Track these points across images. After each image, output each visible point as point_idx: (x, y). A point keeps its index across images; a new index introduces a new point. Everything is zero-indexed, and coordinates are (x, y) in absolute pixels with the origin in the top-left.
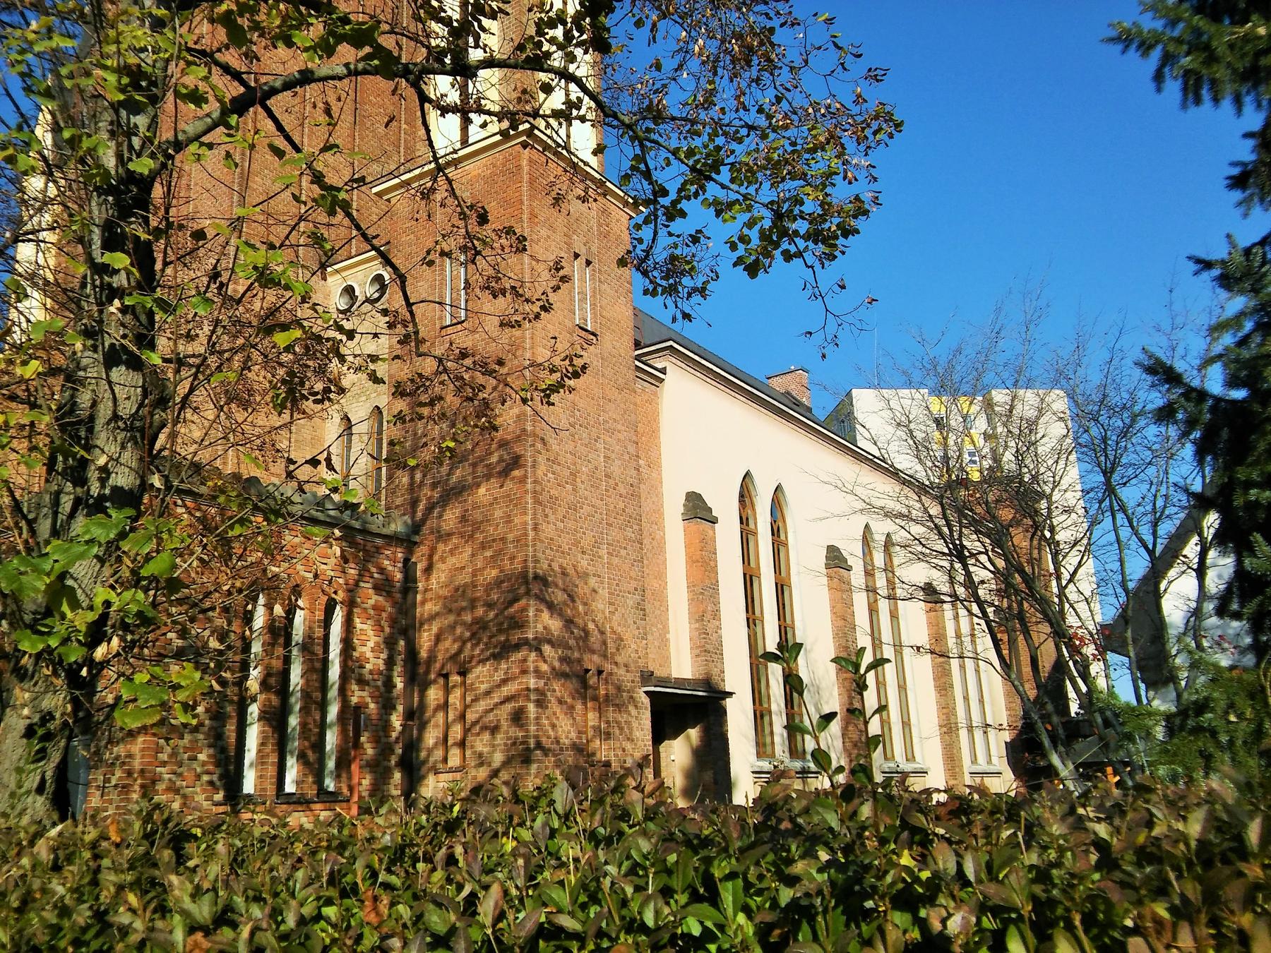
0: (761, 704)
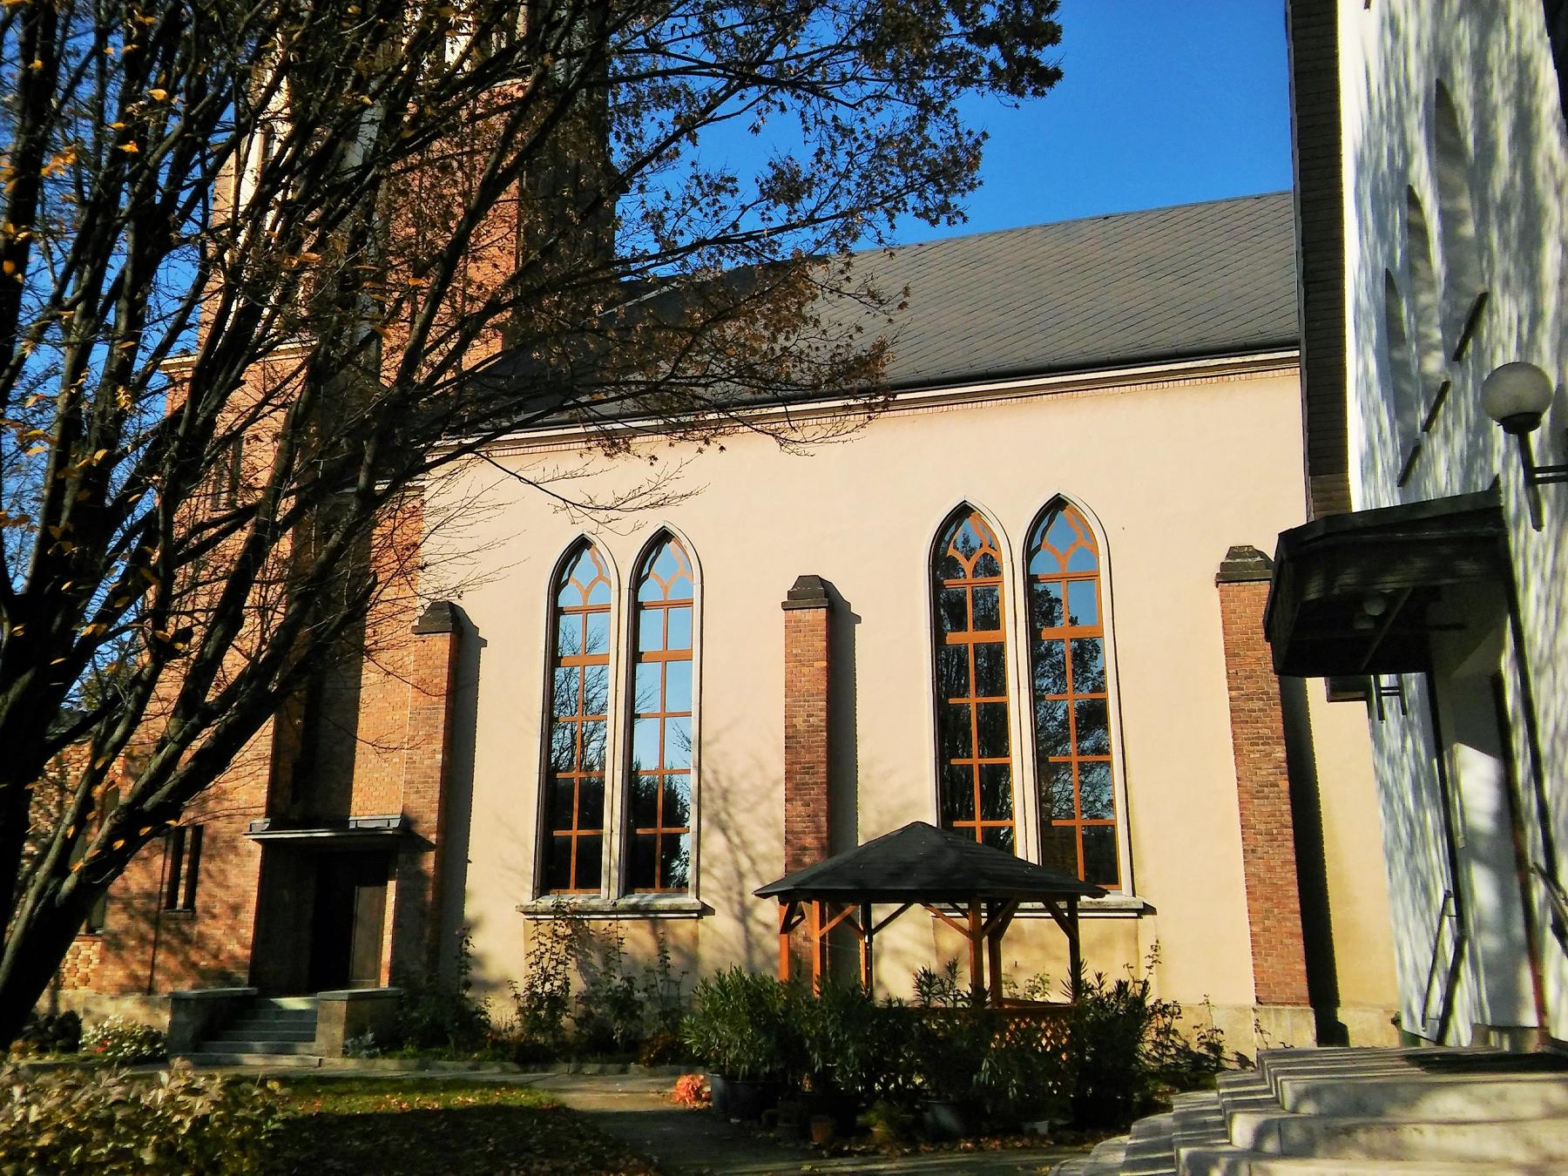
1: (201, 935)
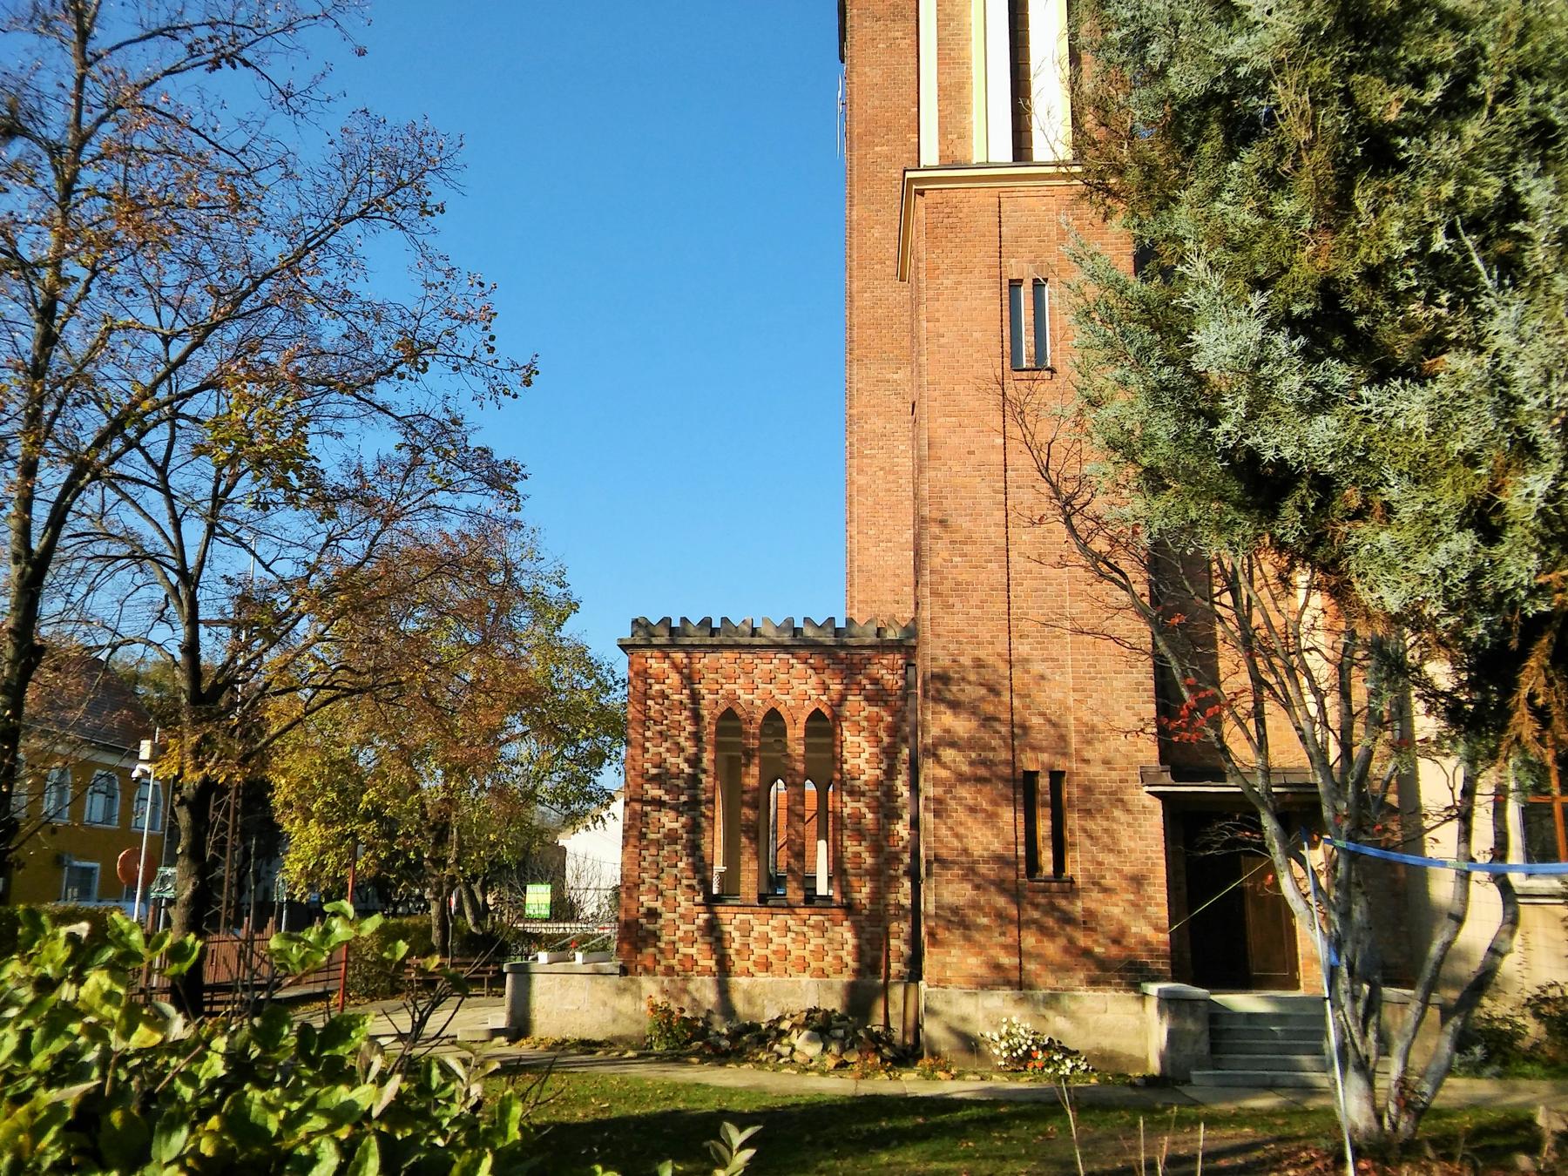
0: (919, 450)
1: (1090, 913)
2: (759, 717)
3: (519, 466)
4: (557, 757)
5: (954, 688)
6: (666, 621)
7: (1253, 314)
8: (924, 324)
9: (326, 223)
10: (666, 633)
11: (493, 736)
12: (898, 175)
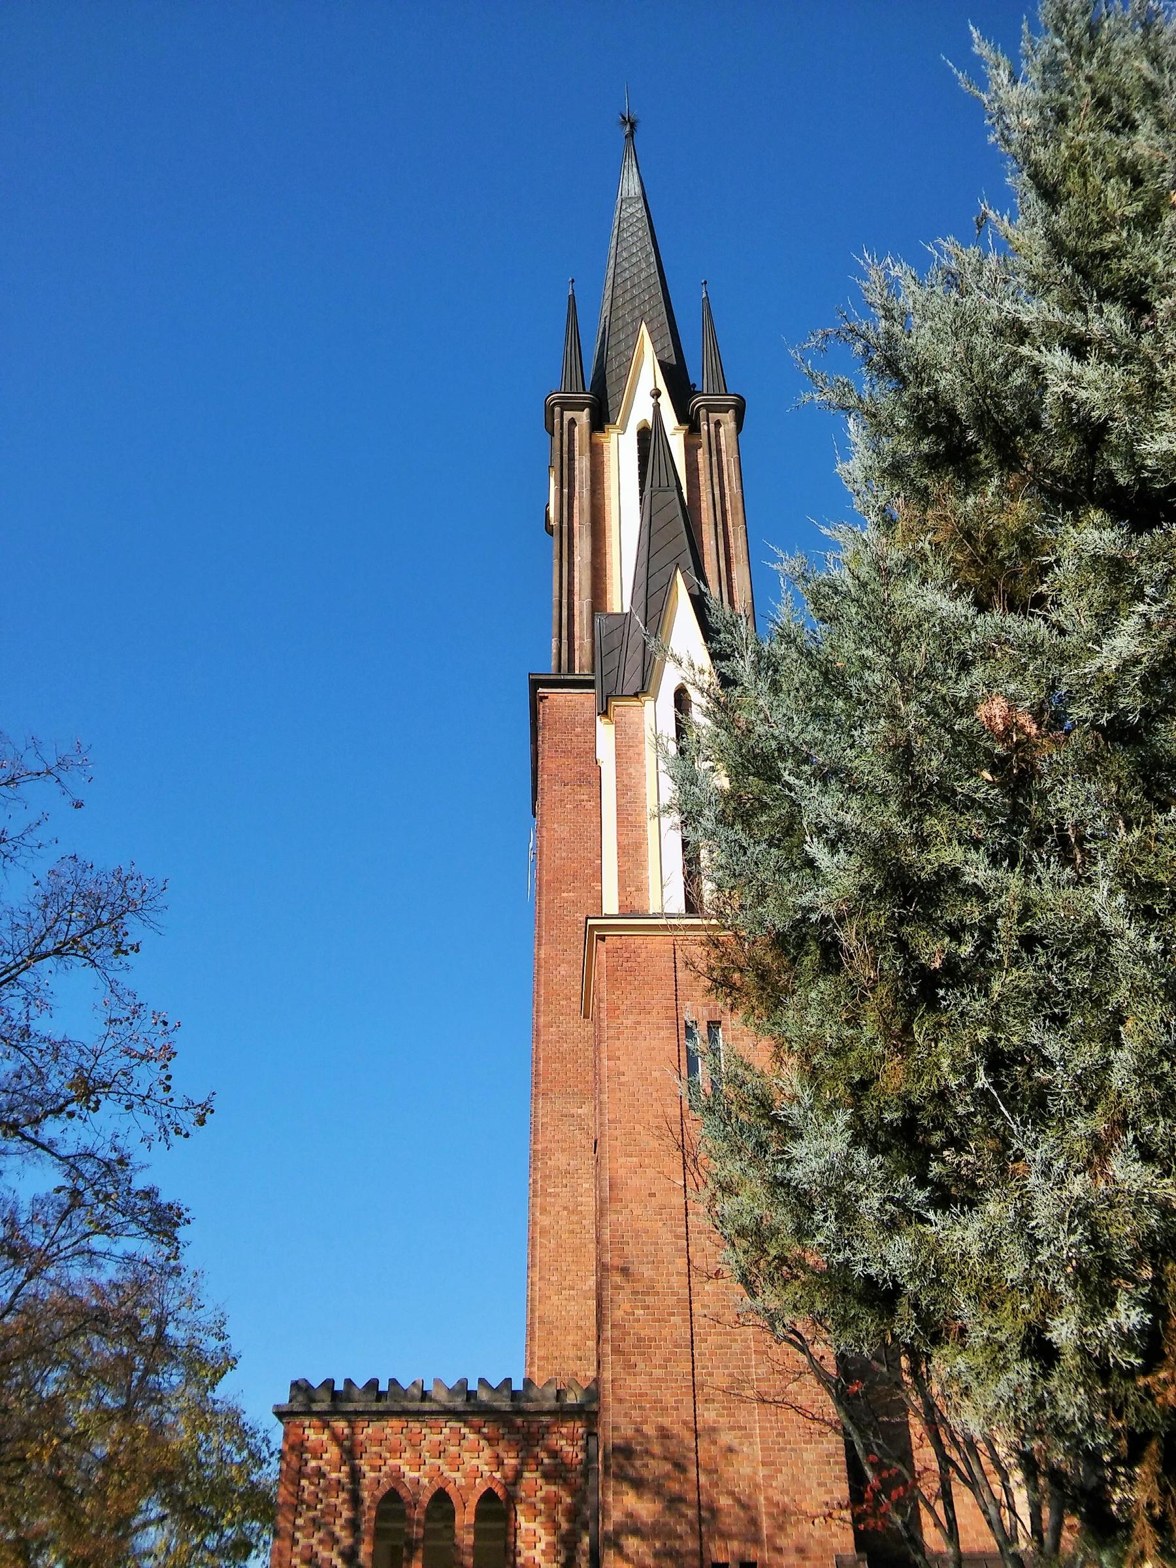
2: (425, 1498)
3: (183, 1210)
4: (197, 1547)
5: (638, 1463)
6: (329, 1384)
7: (839, 1130)
8: (605, 1062)
9: (19, 959)
10: (327, 1397)
11: (124, 1525)
12: (583, 919)
